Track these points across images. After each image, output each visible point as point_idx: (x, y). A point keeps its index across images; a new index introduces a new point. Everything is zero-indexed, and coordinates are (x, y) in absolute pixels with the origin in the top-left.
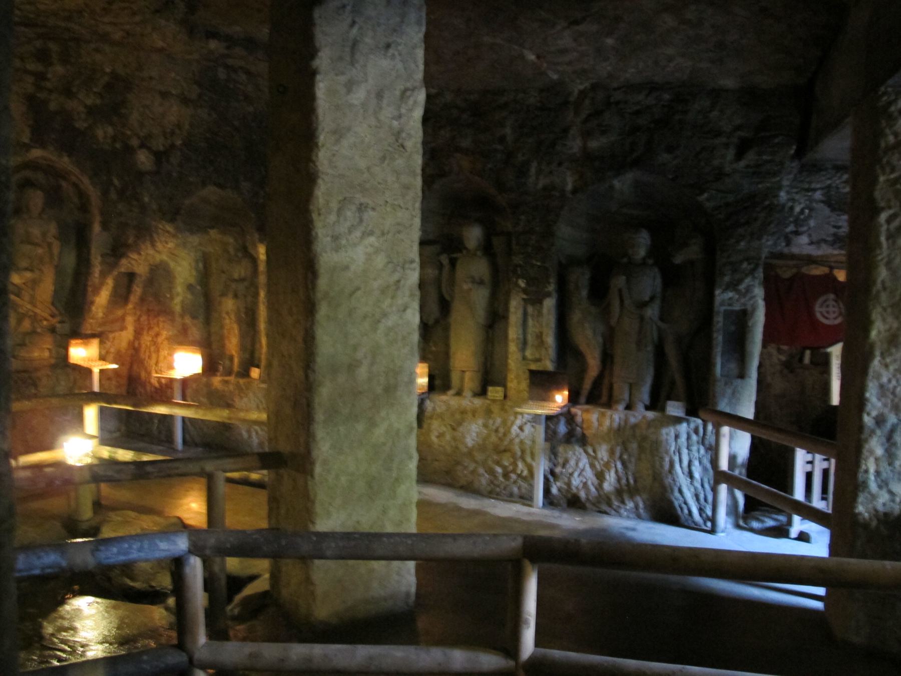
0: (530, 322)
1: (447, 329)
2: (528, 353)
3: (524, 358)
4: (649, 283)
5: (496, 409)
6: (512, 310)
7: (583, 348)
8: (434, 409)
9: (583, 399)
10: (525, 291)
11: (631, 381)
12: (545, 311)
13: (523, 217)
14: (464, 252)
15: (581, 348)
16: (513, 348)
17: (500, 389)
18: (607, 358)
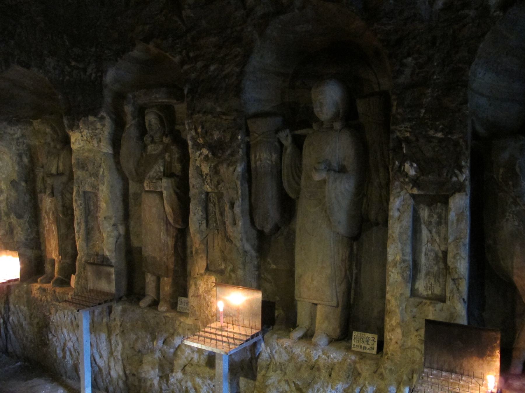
0: (425, 233)
1: (290, 241)
2: (421, 286)
3: (414, 293)
6: (394, 213)
8: (271, 357)
9: (517, 368)
10: (415, 182)
12: (452, 215)
16: (394, 276)
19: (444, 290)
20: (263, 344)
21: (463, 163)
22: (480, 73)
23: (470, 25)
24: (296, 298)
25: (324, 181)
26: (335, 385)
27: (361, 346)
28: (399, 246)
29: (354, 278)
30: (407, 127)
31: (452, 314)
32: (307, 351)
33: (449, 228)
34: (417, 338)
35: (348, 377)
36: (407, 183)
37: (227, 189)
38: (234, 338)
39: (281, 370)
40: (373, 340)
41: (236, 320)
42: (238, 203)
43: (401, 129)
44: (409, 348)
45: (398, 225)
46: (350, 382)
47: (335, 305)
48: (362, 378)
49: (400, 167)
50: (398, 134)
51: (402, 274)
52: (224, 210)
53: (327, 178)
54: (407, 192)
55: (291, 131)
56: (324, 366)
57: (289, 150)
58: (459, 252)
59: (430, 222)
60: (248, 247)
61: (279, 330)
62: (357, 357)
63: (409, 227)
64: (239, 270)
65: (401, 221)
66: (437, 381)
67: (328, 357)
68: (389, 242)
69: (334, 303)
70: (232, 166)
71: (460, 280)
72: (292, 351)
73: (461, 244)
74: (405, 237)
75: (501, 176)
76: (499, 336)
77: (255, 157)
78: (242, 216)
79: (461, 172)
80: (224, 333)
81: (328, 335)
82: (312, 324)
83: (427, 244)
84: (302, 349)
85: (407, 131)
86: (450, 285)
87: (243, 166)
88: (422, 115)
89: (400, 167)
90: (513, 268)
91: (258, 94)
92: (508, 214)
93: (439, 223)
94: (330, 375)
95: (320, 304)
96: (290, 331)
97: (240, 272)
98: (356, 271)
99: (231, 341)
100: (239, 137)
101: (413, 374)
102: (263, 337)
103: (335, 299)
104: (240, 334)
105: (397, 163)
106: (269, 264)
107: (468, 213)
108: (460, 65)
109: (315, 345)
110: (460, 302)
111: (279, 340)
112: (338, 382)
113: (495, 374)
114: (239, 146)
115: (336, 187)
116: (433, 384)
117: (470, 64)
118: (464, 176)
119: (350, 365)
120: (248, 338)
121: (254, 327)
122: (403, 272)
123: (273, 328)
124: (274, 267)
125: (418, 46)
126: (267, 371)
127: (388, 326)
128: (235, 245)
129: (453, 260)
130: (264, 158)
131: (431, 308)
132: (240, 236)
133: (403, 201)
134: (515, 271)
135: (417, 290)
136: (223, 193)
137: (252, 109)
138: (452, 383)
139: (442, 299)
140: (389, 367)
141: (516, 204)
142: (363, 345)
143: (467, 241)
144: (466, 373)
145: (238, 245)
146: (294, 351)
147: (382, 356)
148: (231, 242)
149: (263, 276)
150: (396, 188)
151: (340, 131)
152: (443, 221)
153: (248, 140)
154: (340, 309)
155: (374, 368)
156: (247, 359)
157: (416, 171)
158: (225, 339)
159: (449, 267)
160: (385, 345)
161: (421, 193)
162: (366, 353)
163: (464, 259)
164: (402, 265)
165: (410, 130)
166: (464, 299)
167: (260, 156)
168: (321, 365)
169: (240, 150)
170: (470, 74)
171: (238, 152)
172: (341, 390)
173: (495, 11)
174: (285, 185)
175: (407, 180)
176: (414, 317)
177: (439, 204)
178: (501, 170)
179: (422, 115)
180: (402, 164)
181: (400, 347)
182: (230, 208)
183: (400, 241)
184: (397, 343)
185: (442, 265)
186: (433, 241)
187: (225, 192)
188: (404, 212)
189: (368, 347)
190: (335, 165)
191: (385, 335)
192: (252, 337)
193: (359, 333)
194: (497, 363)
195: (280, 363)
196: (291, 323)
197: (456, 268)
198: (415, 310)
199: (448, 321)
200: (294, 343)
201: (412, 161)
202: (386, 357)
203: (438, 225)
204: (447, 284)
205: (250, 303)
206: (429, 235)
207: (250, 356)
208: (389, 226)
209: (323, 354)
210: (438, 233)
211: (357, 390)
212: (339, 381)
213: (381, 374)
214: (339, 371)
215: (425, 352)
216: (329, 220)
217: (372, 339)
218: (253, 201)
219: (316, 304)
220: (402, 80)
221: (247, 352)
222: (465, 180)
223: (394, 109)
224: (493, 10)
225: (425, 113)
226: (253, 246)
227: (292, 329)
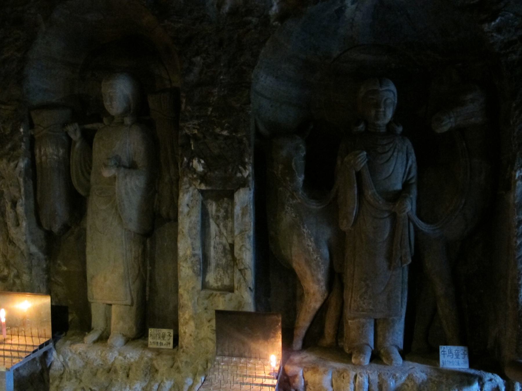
0: (213, 228)
1: (81, 239)
2: (211, 278)
3: (205, 286)
4: (399, 166)
5: (162, 364)
6: (183, 209)
7: (299, 266)
8: (65, 365)
9: (298, 344)
10: (203, 178)
11: (379, 316)
12: (237, 210)
13: (198, 59)
14: (105, 120)
15: (295, 265)
16: (186, 271)
17: (167, 332)
18: (335, 280)
19: (232, 280)
20: (54, 353)
21: (247, 160)
22: (262, 77)
23: (253, 31)
24: (89, 300)
25: (114, 178)
26: (133, 385)
27: (157, 343)
28: (189, 241)
29: (148, 275)
30: (195, 125)
31: (240, 303)
32: (103, 355)
33: (235, 222)
34: (209, 329)
35: (146, 375)
36: (196, 179)
37: (8, 186)
38: (18, 351)
39: (76, 378)
40: (169, 335)
41: (22, 330)
42: (21, 202)
43: (190, 126)
44: (202, 339)
45: (188, 220)
46: (148, 380)
47: (129, 303)
48: (159, 375)
49: (188, 163)
50: (187, 131)
51: (192, 267)
52: (5, 211)
53: (116, 174)
54: (196, 188)
55: (79, 125)
56: (121, 367)
57: (78, 145)
58: (244, 243)
59: (218, 217)
60: (34, 249)
61: (73, 335)
62: (154, 354)
63: (198, 221)
64: (25, 275)
65: (190, 216)
66: (227, 367)
67: (125, 357)
68: (179, 237)
69: (129, 302)
70: (13, 161)
71: (246, 270)
72: (87, 357)
73: (246, 236)
74: (194, 232)
75: (279, 172)
76: (280, 318)
77: (40, 151)
78: (26, 216)
79: (245, 168)
80: (7, 347)
81: (124, 335)
82: (107, 326)
83: (215, 238)
84: (97, 353)
85: (194, 128)
86: (237, 275)
87: (26, 161)
88: (209, 113)
89: (188, 163)
90: (291, 256)
91: (43, 83)
92: (286, 207)
93: (226, 218)
94: (128, 376)
95: (114, 304)
96: (85, 335)
97: (26, 278)
98: (150, 268)
99: (15, 354)
100: (22, 130)
101: (207, 364)
102: (54, 345)
103: (129, 298)
104: (26, 345)
105: (185, 159)
106: (59, 265)
107: (251, 207)
108: (244, 68)
109: (111, 347)
110: (246, 291)
111: (72, 346)
112: (135, 381)
113: (278, 353)
114: (21, 140)
115: (126, 184)
116: (223, 371)
117: (253, 67)
118: (248, 172)
119: (147, 363)
120: (35, 348)
121: (44, 336)
122: (193, 266)
123: (66, 334)
124: (65, 268)
125: (206, 46)
126: (60, 382)
127: (181, 321)
128: (19, 248)
129: (239, 252)
130: (49, 153)
131: (221, 299)
132: (24, 238)
133: (192, 196)
134: (294, 258)
135: (208, 282)
136: (3, 191)
137: (37, 99)
138: (241, 367)
139: (231, 289)
140: (185, 360)
141: (293, 197)
142: (159, 341)
143: (251, 233)
144: (253, 356)
145: (23, 247)
146: (89, 356)
147: (178, 350)
148: (14, 244)
149: (53, 279)
150: (185, 184)
151: (131, 126)
152: (229, 215)
153: (32, 133)
154: (134, 308)
155: (170, 363)
156: (38, 372)
157: (203, 168)
158: (7, 353)
159: (236, 258)
160: (180, 338)
161: (209, 188)
162: (162, 349)
163: (249, 250)
164: (192, 259)
165: (198, 127)
166: (250, 288)
167: (45, 150)
168: (118, 367)
169: (23, 144)
170: (252, 77)
171: (21, 146)
172: (140, 390)
173: (274, 22)
174: (75, 182)
175: (195, 176)
176: (205, 309)
177: (225, 199)
178: (280, 167)
179: (209, 113)
180: (190, 160)
181: (194, 339)
182: (12, 207)
183: (190, 236)
184: (191, 335)
185: (229, 257)
186: (221, 234)
187: (5, 190)
188: (193, 207)
189: (164, 342)
190: (125, 161)
191: (179, 329)
192: (41, 347)
193: (155, 329)
194: (279, 343)
195: (75, 371)
196: (85, 326)
197: (242, 259)
198: (206, 302)
199: (236, 310)
200: (89, 347)
201: (200, 158)
202: (182, 350)
203: (225, 220)
204: (235, 274)
205: (38, 310)
206: (217, 228)
207: (40, 368)
208: (179, 221)
209: (120, 355)
210: (225, 227)
211: (155, 387)
212: (137, 380)
213: (178, 368)
214: (137, 370)
215: (217, 342)
216: (120, 217)
217: (167, 334)
218: (38, 199)
219: (111, 305)
220: (192, 78)
221: (36, 364)
222: (249, 175)
223: (183, 106)
224: (272, 20)
225: (212, 112)
226: (40, 248)
227: (87, 333)
